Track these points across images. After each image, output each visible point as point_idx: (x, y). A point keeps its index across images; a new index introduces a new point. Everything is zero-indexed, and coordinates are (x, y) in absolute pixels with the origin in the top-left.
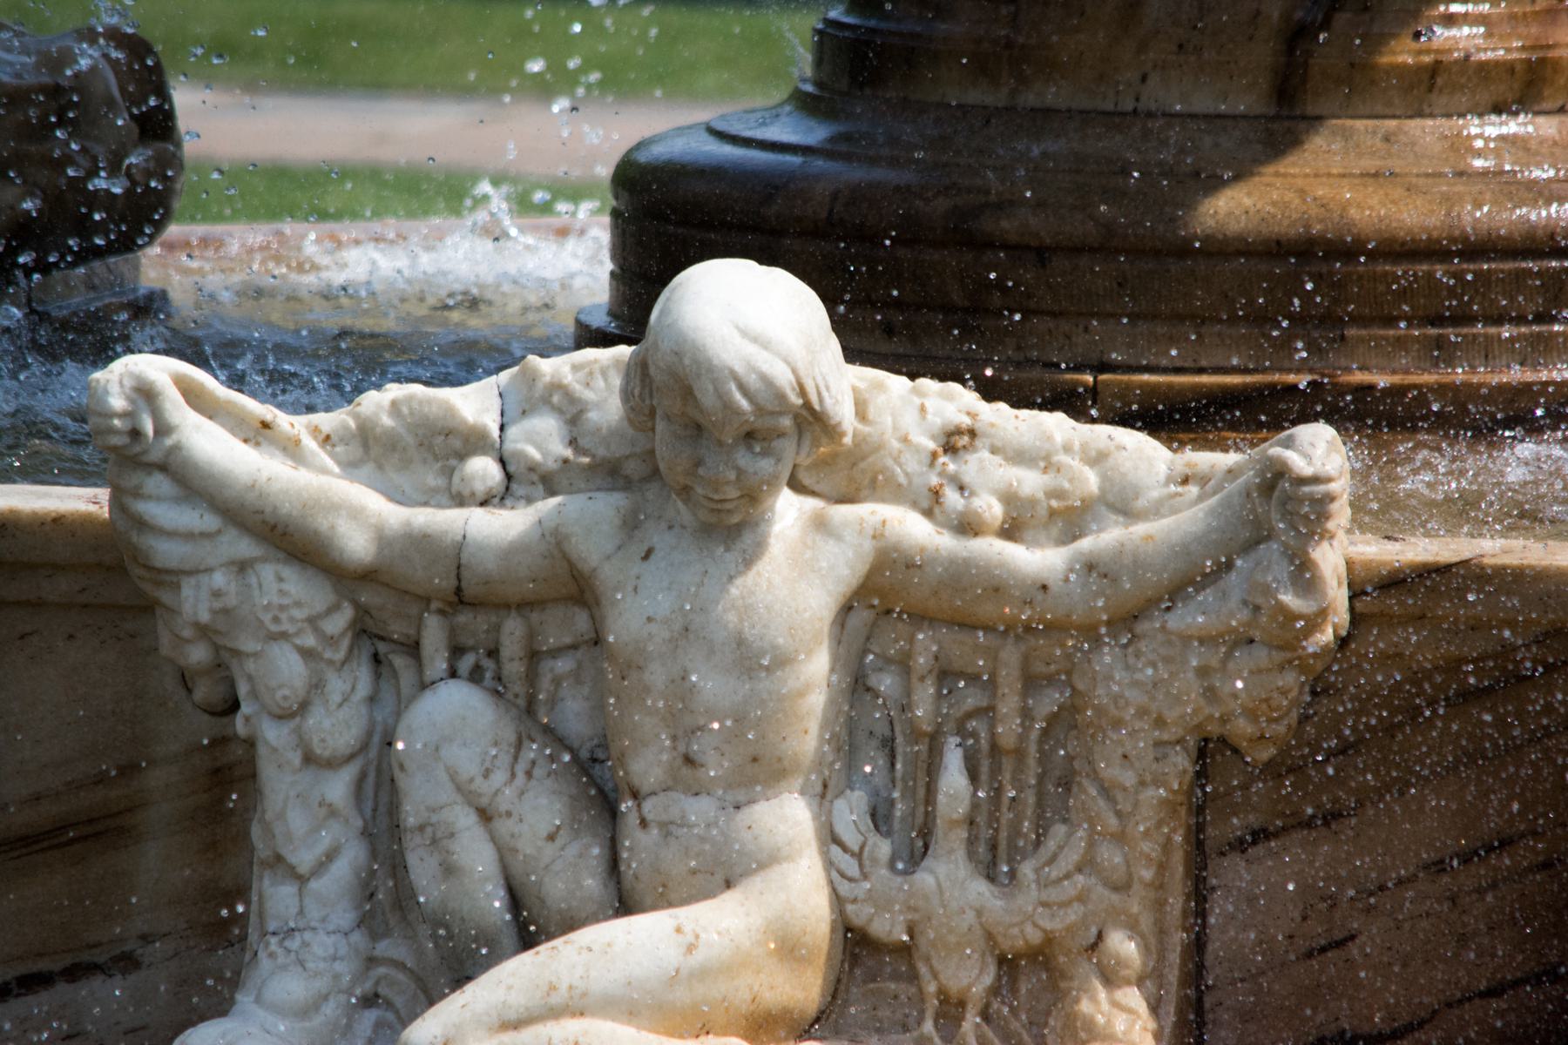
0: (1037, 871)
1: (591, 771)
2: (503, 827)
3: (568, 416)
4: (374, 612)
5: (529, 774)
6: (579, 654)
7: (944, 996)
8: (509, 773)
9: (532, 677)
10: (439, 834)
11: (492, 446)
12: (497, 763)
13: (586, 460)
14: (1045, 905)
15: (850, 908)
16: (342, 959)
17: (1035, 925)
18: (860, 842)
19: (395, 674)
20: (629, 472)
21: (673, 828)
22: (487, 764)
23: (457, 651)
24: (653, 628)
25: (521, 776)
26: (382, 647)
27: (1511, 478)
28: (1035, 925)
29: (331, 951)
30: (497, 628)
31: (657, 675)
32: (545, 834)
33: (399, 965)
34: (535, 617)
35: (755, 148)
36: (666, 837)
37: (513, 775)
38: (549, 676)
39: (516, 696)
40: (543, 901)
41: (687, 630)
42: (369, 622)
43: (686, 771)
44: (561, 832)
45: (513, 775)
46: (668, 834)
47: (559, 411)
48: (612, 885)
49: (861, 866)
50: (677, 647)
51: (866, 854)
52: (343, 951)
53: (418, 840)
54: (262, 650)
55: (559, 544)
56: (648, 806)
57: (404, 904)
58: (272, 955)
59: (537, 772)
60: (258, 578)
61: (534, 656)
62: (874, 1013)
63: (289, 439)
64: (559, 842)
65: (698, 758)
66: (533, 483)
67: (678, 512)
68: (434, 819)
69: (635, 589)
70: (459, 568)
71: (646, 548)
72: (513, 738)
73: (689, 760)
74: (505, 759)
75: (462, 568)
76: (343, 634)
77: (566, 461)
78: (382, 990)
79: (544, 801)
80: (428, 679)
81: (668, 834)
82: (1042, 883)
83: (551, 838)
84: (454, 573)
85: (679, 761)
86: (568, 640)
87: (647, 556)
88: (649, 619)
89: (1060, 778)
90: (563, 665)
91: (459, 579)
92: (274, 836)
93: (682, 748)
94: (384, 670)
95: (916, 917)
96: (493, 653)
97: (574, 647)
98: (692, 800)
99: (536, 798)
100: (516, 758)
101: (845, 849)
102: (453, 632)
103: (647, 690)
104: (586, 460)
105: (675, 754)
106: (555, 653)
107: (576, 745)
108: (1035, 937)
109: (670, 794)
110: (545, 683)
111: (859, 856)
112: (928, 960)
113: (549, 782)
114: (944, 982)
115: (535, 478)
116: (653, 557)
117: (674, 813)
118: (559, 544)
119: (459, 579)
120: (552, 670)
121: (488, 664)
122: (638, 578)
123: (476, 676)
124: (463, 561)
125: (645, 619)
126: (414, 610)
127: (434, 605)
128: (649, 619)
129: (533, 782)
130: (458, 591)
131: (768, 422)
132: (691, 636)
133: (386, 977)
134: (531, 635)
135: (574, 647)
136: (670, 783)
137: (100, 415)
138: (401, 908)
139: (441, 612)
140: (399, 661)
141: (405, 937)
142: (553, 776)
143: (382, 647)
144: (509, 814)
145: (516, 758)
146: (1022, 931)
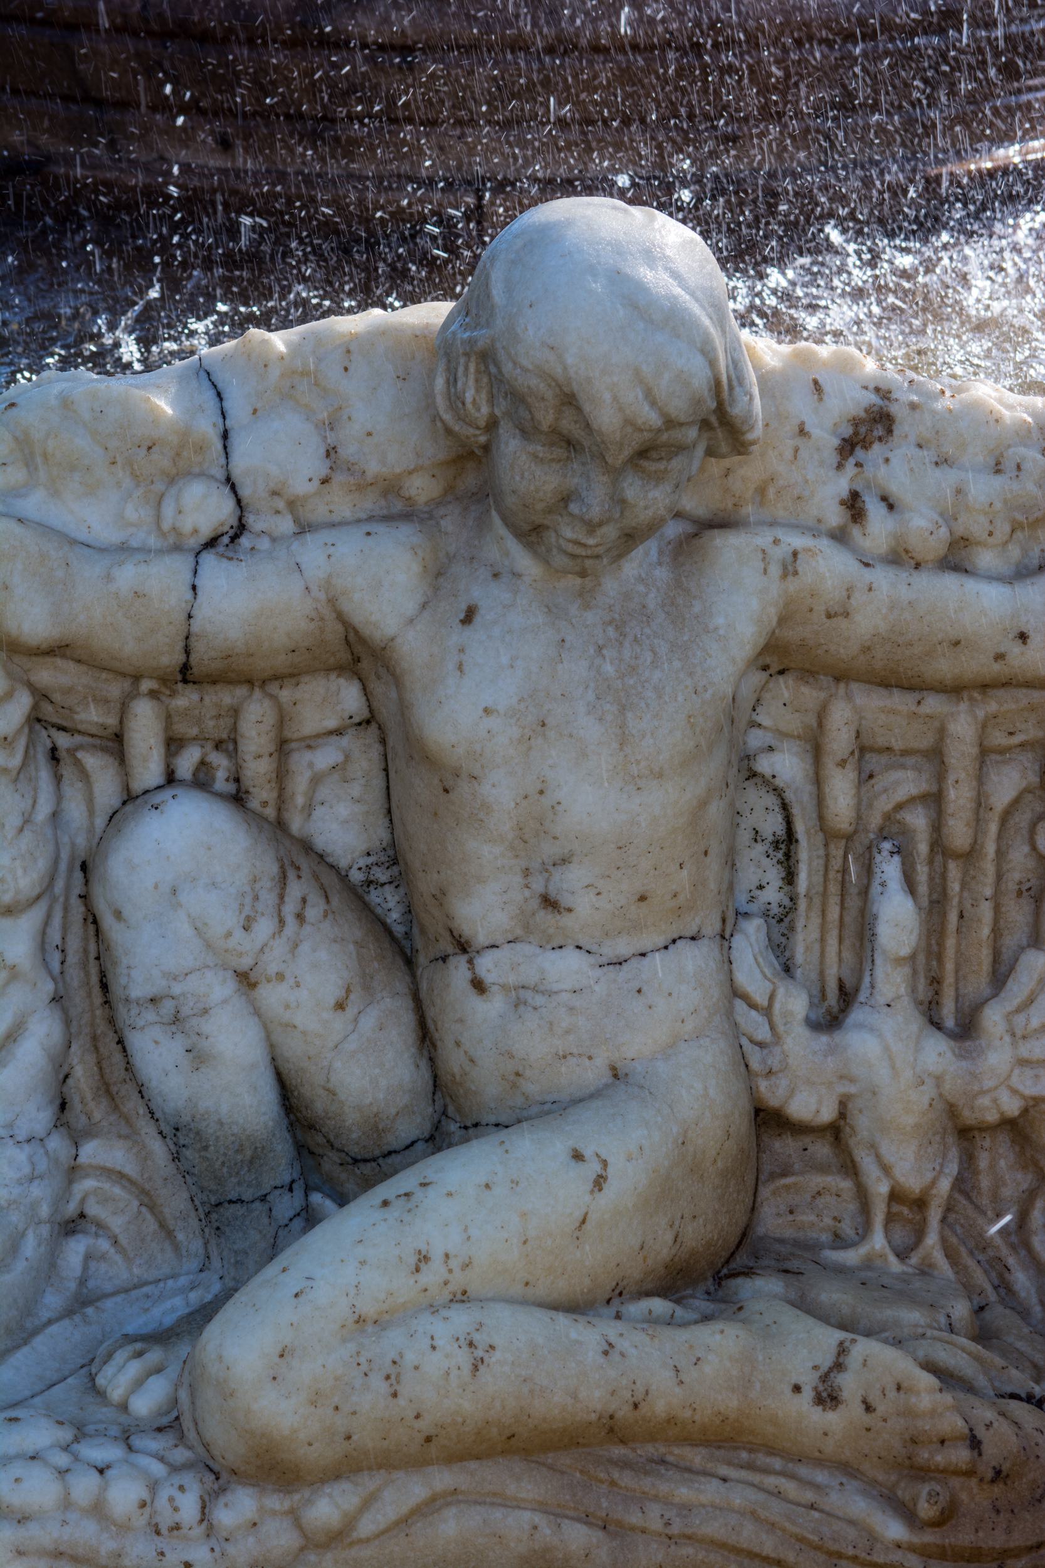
0: (1009, 1017)
1: (367, 898)
2: (272, 996)
4: (57, 697)
5: (300, 917)
6: (345, 741)
7: (895, 1196)
8: (276, 920)
9: (281, 775)
10: (185, 1011)
12: (260, 907)
14: (1023, 1062)
15: (763, 1085)
16: (41, 1177)
17: (1014, 1091)
18: (768, 991)
19: (84, 775)
20: (413, 492)
22: (247, 910)
23: (173, 744)
24: (492, 722)
25: (290, 920)
26: (63, 741)
27: (687, 200)
28: (1014, 1091)
29: (27, 1170)
30: (235, 712)
32: (332, 1002)
33: (120, 1177)
34: (285, 695)
37: (282, 922)
38: (308, 774)
39: (265, 804)
40: (332, 1093)
41: (544, 725)
42: (48, 710)
43: (546, 918)
44: (352, 997)
45: (282, 922)
46: (518, 1004)
48: (424, 1063)
49: (772, 1028)
50: (530, 749)
51: (777, 1006)
52: (43, 1165)
53: (150, 1015)
55: (332, 601)
56: (488, 965)
57: (114, 1089)
59: (312, 913)
61: (282, 748)
62: (790, 1218)
64: (351, 1011)
65: (566, 900)
66: (278, 512)
67: (507, 554)
68: (177, 989)
69: (460, 667)
70: (187, 638)
71: (464, 607)
72: (275, 869)
73: (549, 903)
74: (268, 898)
75: (192, 639)
76: (19, 731)
78: (93, 1209)
79: (323, 955)
80: (137, 786)
81: (518, 1004)
82: (1019, 1033)
83: (340, 1006)
84: (180, 645)
85: (535, 903)
86: (332, 723)
87: (469, 617)
88: (487, 711)
89: (1020, 883)
90: (325, 757)
91: (187, 651)
93: (538, 885)
94: (67, 771)
95: (852, 1089)
96: (228, 744)
97: (338, 732)
99: (314, 951)
100: (281, 897)
101: (753, 1006)
102: (168, 719)
105: (527, 893)
106: (311, 743)
107: (343, 863)
108: (1012, 1106)
109: (518, 946)
110: (299, 785)
111: (767, 1012)
112: (873, 1147)
113: (326, 926)
114: (902, 1180)
115: (281, 504)
116: (477, 619)
117: (529, 975)
118: (332, 601)
119: (187, 651)
120: (311, 765)
121: (221, 763)
122: (462, 650)
123: (201, 781)
125: (480, 712)
126: (115, 689)
127: (146, 685)
128: (487, 711)
129: (307, 929)
130: (185, 668)
131: (677, 435)
133: (96, 1191)
134: (282, 720)
135: (338, 732)
136: (519, 932)
138: (108, 1091)
139: (153, 694)
140: (92, 761)
141: (120, 1137)
142: (330, 916)
143: (63, 741)
144: (281, 977)
145: (281, 897)
146: (995, 1101)
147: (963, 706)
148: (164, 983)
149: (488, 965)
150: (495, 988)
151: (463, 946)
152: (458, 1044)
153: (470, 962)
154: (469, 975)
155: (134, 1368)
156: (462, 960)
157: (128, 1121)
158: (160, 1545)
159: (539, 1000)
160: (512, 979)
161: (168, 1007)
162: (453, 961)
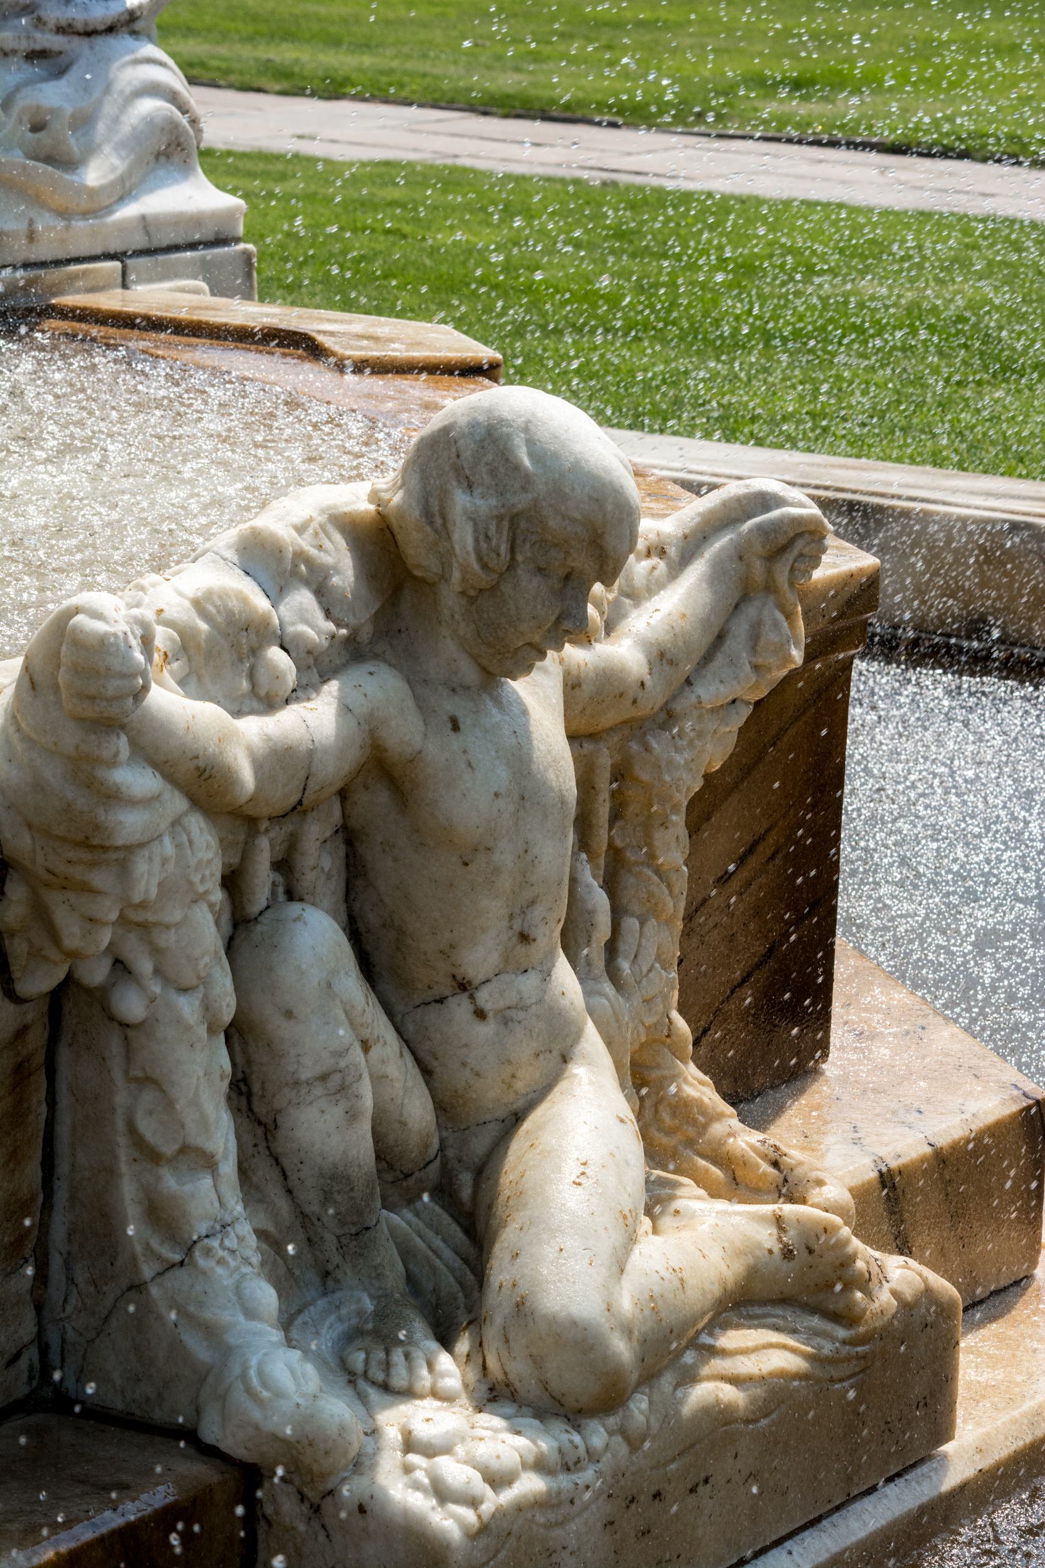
3: (314, 586)
11: (274, 632)
13: (344, 631)
21: (512, 1013)
24: (500, 803)
31: (505, 856)
35: (73, 310)
36: (506, 1024)
40: (403, 1124)
47: (307, 583)
53: (318, 1090)
54: (186, 917)
56: (484, 998)
58: (221, 1262)
60: (188, 835)
63: (376, 657)
68: (342, 1064)
69: (470, 765)
77: (333, 637)
85: (515, 939)
88: (496, 795)
92: (183, 1126)
93: (517, 927)
98: (522, 978)
103: (497, 871)
104: (344, 631)
105: (511, 933)
109: (502, 977)
117: (511, 998)
118: (372, 732)
124: (313, 770)
128: (496, 795)
132: (528, 805)
137: (124, 676)
147: (602, 745)
148: (332, 1061)
149: (484, 998)
150: (491, 1014)
151: (464, 986)
152: (464, 1064)
153: (472, 997)
154: (471, 1008)
155: (424, 1372)
156: (464, 998)
157: (257, 1188)
158: (642, 1498)
159: (521, 1015)
160: (502, 1004)
161: (336, 1079)
162: (452, 1002)
